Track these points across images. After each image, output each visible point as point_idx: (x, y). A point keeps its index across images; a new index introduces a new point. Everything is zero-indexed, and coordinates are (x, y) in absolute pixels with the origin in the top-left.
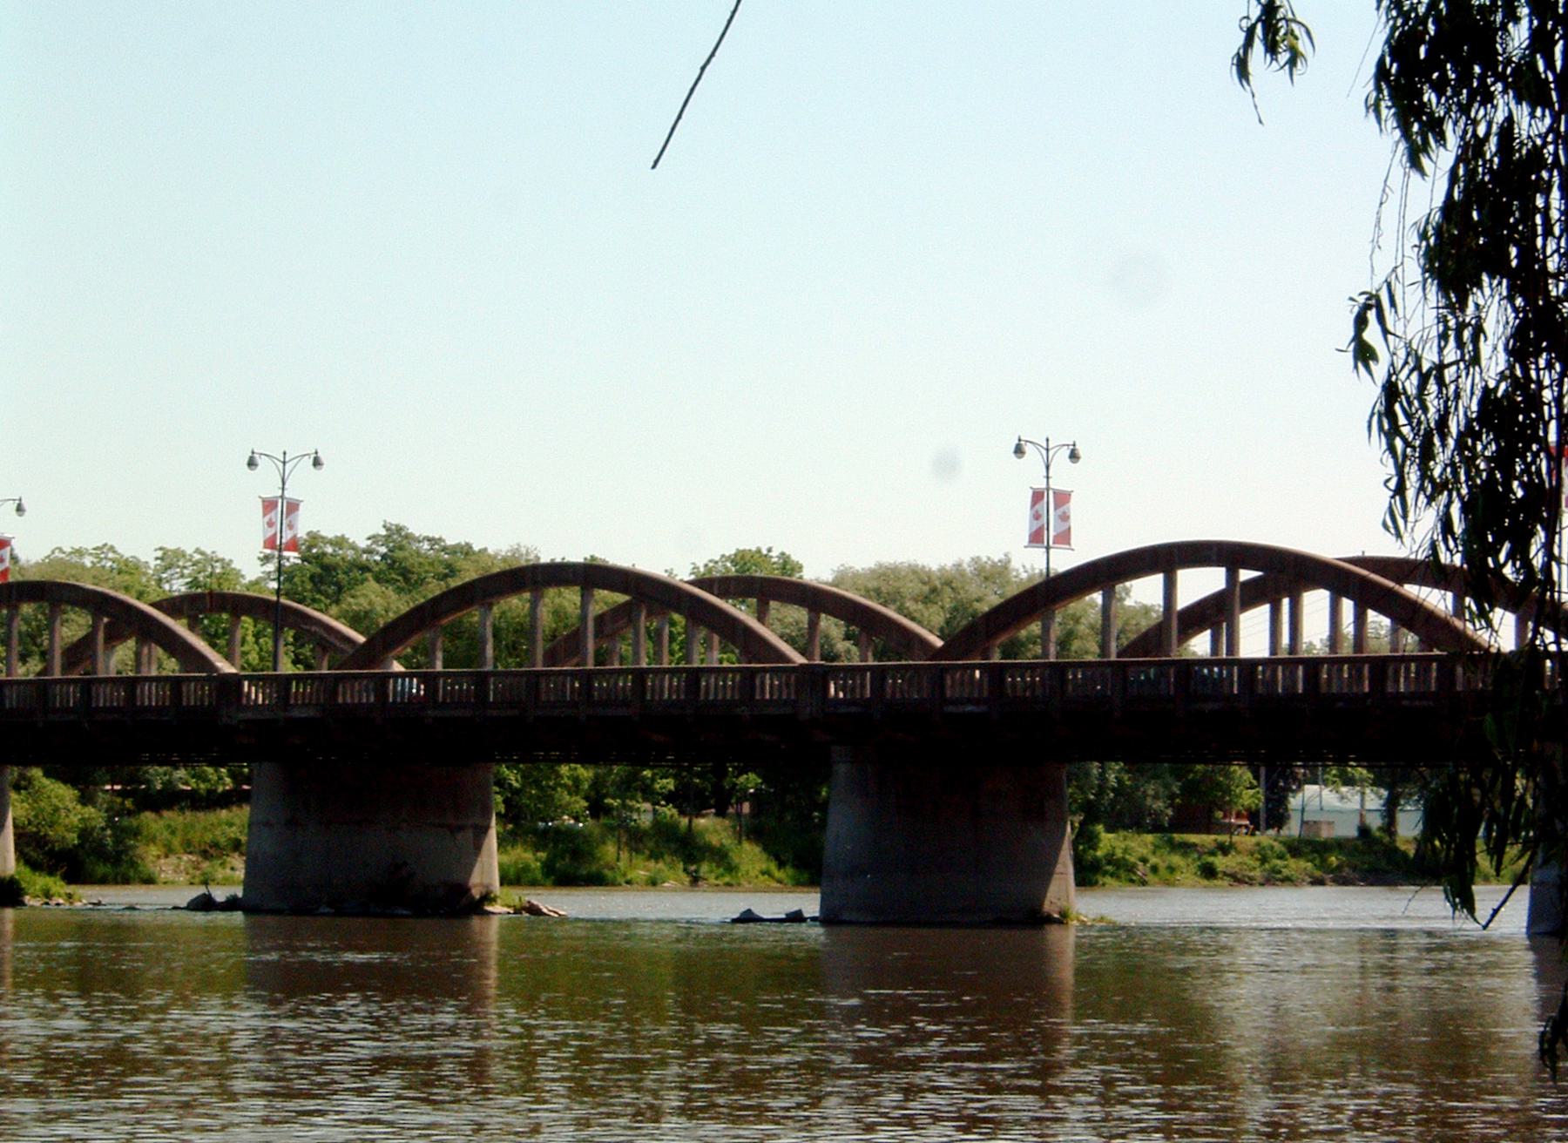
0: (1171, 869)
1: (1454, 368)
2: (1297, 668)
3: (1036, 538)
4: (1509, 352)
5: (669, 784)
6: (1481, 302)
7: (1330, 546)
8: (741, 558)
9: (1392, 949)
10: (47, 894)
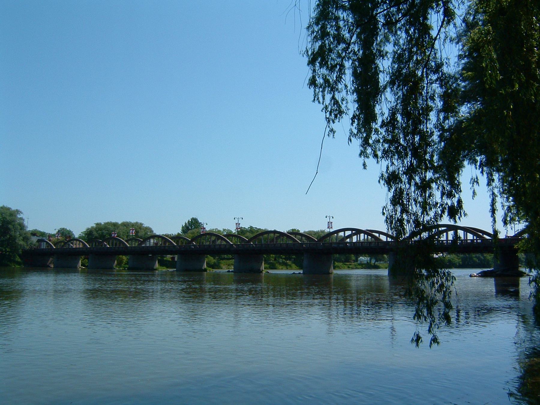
0: (344, 267)
3: (328, 228)
4: (400, 213)
5: (284, 257)
7: (364, 229)
8: (292, 230)
9: (371, 277)
10: (210, 270)
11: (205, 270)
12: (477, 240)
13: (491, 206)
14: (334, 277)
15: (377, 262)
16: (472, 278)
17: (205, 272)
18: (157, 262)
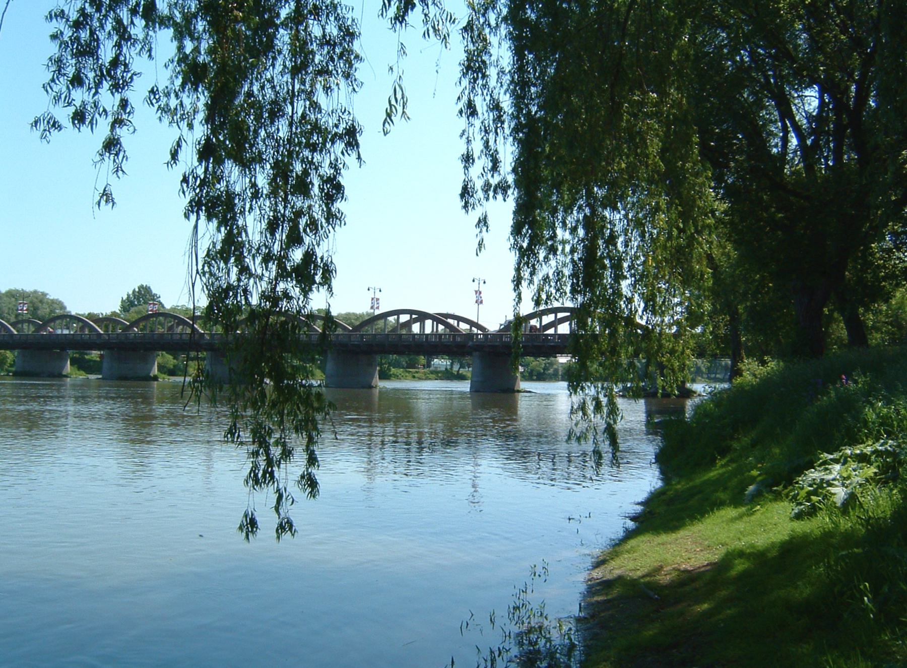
3: (372, 308)
7: (431, 311)
11: (155, 378)
14: (380, 392)
15: (464, 368)
17: (156, 382)
18: (69, 362)
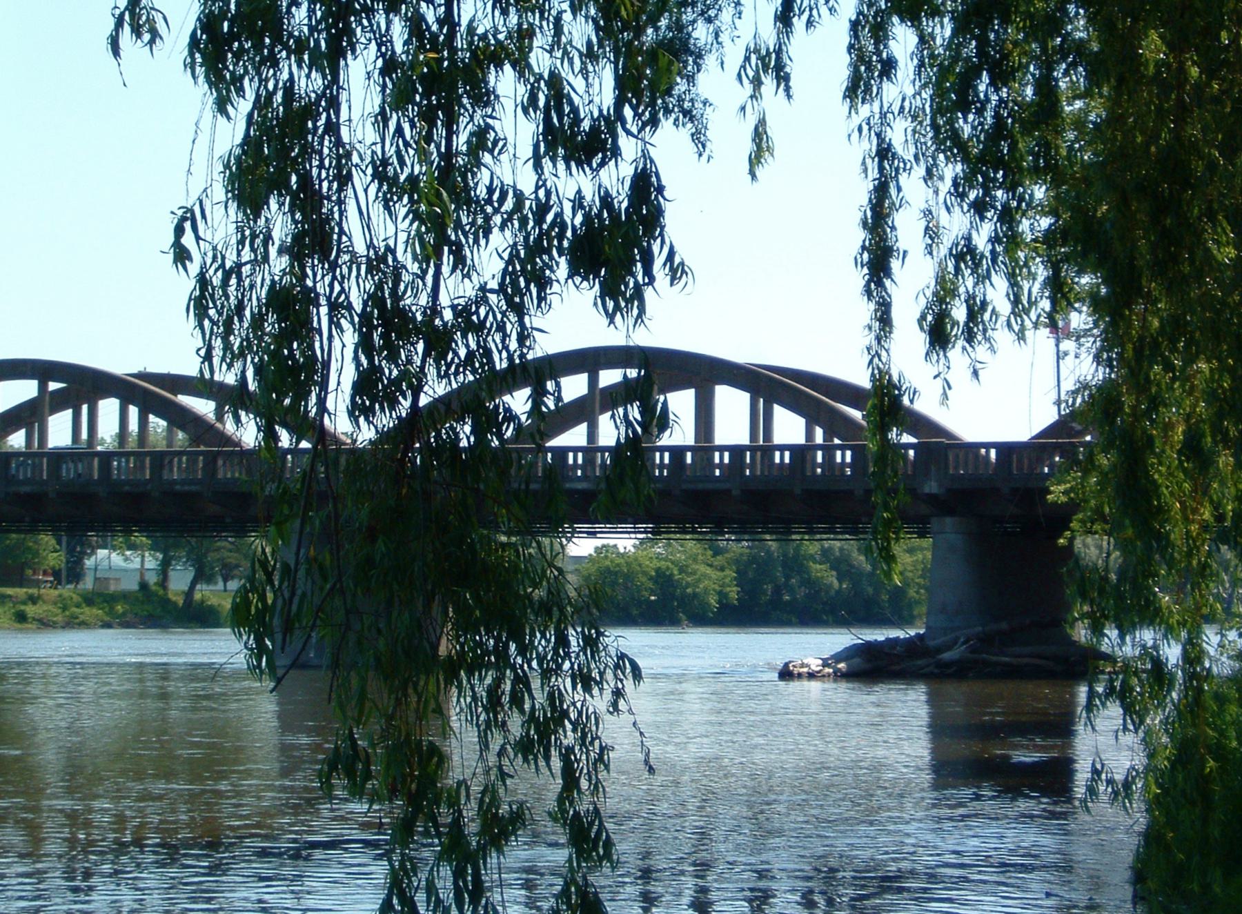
1: (249, 266)
2: (93, 460)
6: (269, 216)
7: (120, 364)
12: (828, 450)
13: (865, 224)
15: (210, 580)
16: (795, 685)
